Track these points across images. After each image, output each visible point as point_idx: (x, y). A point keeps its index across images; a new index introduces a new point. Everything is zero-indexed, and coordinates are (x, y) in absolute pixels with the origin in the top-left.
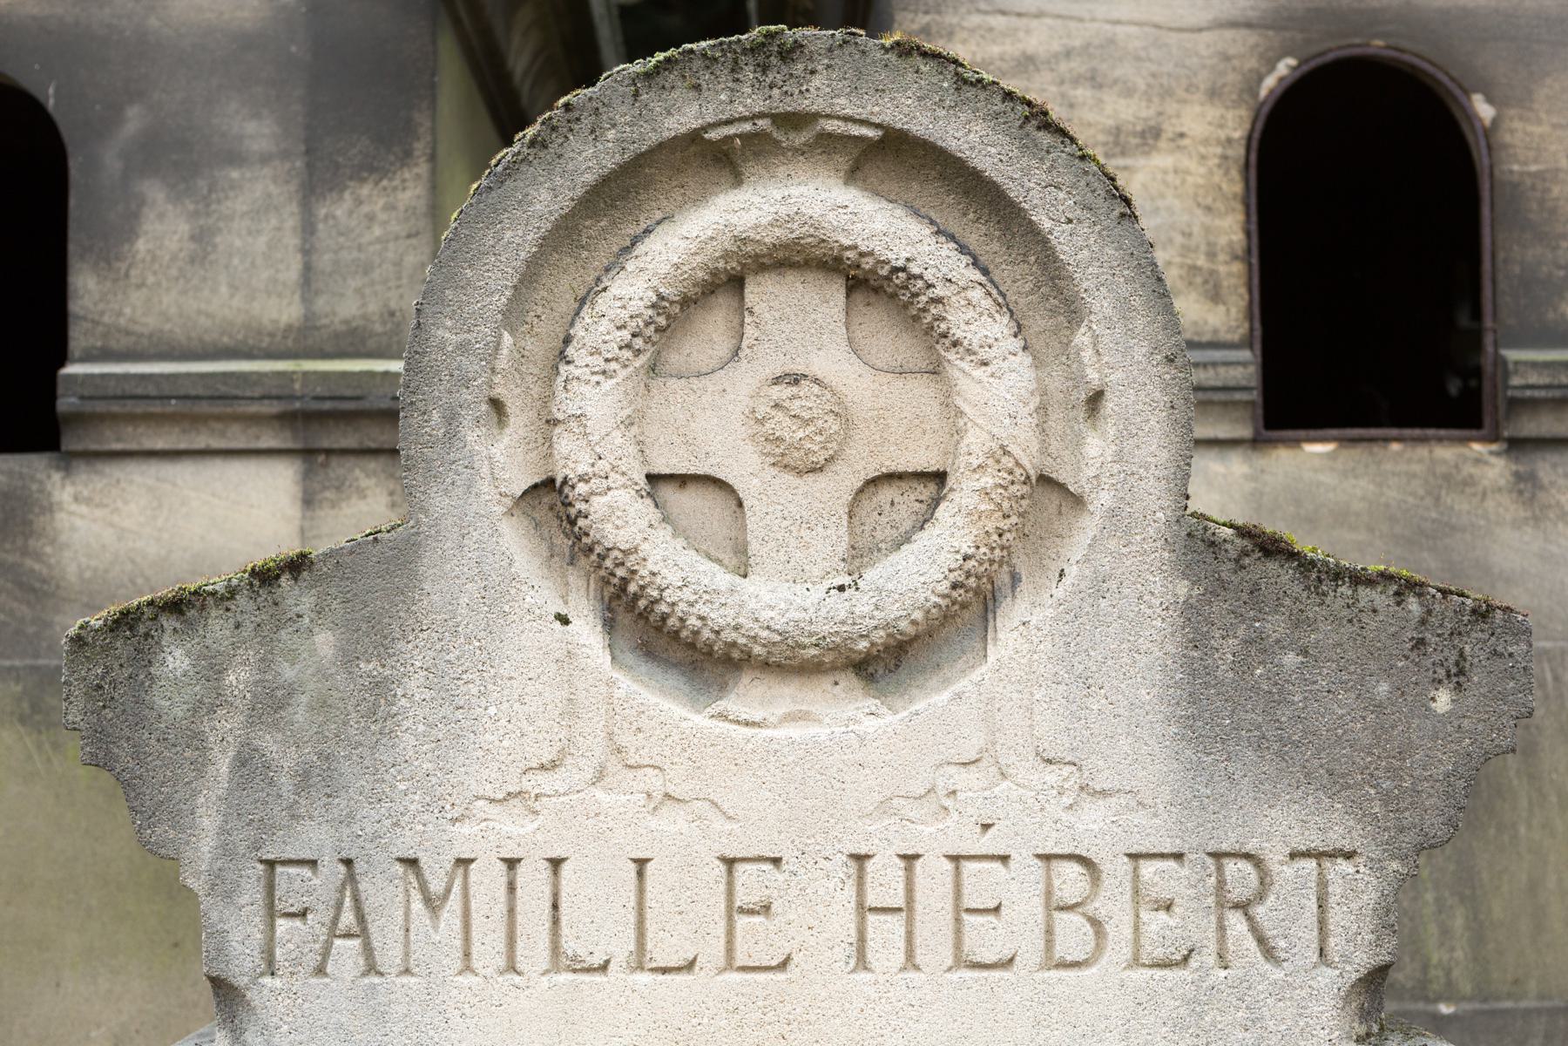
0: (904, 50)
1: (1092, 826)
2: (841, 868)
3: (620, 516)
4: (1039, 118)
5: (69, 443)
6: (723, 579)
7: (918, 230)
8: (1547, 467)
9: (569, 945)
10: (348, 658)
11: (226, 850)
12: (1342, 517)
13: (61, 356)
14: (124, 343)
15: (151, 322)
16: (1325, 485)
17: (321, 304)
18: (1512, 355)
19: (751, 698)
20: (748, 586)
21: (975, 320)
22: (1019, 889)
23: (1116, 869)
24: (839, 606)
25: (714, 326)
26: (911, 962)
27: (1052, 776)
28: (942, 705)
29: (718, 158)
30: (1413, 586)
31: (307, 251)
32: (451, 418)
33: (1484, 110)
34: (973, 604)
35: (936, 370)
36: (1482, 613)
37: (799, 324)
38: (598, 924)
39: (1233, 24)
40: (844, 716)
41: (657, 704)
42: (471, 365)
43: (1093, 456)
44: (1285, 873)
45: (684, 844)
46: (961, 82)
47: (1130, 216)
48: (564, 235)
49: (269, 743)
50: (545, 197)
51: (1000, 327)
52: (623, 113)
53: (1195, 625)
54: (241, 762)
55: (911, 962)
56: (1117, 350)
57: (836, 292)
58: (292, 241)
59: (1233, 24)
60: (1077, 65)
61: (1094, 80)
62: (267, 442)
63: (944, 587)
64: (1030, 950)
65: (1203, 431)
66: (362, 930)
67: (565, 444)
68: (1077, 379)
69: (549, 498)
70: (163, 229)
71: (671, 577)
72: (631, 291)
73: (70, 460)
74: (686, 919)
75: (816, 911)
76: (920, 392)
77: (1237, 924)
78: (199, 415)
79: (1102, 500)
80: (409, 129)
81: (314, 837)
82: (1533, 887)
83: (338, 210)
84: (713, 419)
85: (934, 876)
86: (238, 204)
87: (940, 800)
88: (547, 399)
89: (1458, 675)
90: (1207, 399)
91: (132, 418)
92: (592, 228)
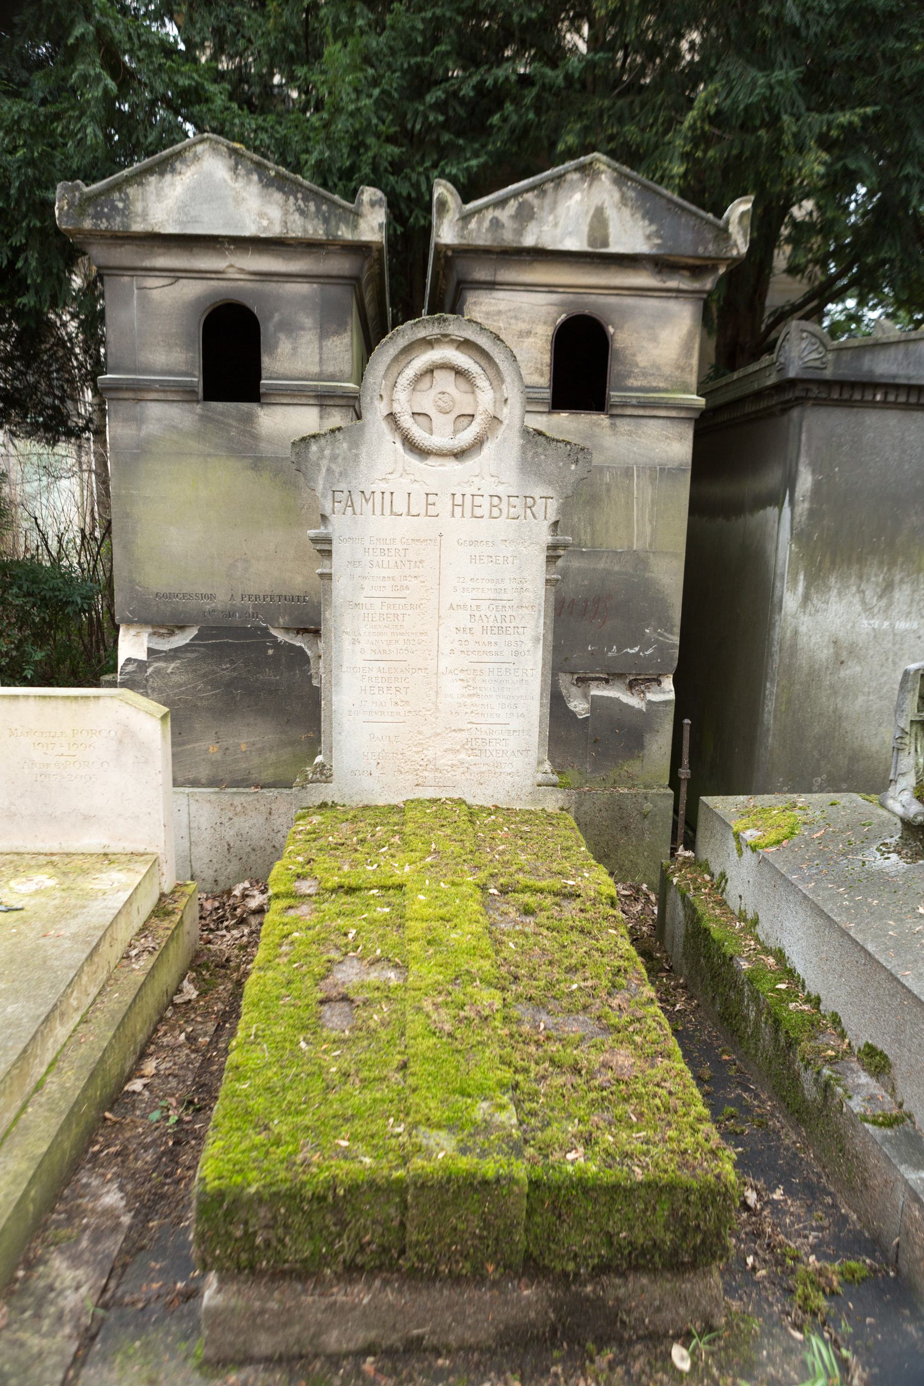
0: (470, 321)
1: (501, 490)
2: (449, 496)
3: (406, 421)
4: (498, 338)
5: (263, 400)
6: (427, 435)
7: (471, 361)
8: (618, 421)
9: (394, 510)
10: (350, 449)
11: (324, 488)
12: (568, 432)
13: (260, 379)
14: (274, 375)
15: (282, 371)
16: (565, 424)
17: (324, 367)
18: (612, 393)
19: (432, 461)
20: (433, 437)
21: (482, 382)
22: (485, 502)
23: (505, 499)
24: (451, 442)
26: (463, 516)
27: (493, 479)
28: (471, 464)
29: (428, 343)
30: (569, 443)
31: (320, 354)
32: (372, 398)
33: (611, 330)
34: (478, 443)
35: (473, 392)
36: (582, 449)
37: (444, 379)
38: (400, 505)
39: (551, 304)
40: (452, 465)
41: (413, 461)
42: (376, 387)
43: (505, 413)
44: (539, 501)
45: (419, 491)
46: (481, 329)
47: (515, 360)
48: (396, 359)
49: (333, 466)
51: (487, 383)
52: (409, 332)
54: (328, 470)
55: (463, 516)
56: (512, 390)
57: (453, 374)
58: (317, 351)
59: (551, 304)
60: (512, 314)
61: (516, 318)
62: (312, 402)
64: (487, 515)
65: (528, 409)
66: (352, 506)
67: (395, 405)
68: (502, 396)
69: (392, 417)
70: (284, 346)
71: (417, 434)
72: (410, 372)
73: (262, 405)
74: (418, 506)
75: (444, 505)
76: (469, 397)
77: (528, 511)
78: (295, 394)
79: (506, 422)
80: (346, 323)
81: (343, 486)
82: (607, 523)
83: (328, 343)
84: (426, 402)
85: (468, 498)
86: (303, 340)
87: (470, 483)
88: (391, 395)
89: (577, 462)
90: (530, 400)
91: (279, 395)
92: (402, 357)
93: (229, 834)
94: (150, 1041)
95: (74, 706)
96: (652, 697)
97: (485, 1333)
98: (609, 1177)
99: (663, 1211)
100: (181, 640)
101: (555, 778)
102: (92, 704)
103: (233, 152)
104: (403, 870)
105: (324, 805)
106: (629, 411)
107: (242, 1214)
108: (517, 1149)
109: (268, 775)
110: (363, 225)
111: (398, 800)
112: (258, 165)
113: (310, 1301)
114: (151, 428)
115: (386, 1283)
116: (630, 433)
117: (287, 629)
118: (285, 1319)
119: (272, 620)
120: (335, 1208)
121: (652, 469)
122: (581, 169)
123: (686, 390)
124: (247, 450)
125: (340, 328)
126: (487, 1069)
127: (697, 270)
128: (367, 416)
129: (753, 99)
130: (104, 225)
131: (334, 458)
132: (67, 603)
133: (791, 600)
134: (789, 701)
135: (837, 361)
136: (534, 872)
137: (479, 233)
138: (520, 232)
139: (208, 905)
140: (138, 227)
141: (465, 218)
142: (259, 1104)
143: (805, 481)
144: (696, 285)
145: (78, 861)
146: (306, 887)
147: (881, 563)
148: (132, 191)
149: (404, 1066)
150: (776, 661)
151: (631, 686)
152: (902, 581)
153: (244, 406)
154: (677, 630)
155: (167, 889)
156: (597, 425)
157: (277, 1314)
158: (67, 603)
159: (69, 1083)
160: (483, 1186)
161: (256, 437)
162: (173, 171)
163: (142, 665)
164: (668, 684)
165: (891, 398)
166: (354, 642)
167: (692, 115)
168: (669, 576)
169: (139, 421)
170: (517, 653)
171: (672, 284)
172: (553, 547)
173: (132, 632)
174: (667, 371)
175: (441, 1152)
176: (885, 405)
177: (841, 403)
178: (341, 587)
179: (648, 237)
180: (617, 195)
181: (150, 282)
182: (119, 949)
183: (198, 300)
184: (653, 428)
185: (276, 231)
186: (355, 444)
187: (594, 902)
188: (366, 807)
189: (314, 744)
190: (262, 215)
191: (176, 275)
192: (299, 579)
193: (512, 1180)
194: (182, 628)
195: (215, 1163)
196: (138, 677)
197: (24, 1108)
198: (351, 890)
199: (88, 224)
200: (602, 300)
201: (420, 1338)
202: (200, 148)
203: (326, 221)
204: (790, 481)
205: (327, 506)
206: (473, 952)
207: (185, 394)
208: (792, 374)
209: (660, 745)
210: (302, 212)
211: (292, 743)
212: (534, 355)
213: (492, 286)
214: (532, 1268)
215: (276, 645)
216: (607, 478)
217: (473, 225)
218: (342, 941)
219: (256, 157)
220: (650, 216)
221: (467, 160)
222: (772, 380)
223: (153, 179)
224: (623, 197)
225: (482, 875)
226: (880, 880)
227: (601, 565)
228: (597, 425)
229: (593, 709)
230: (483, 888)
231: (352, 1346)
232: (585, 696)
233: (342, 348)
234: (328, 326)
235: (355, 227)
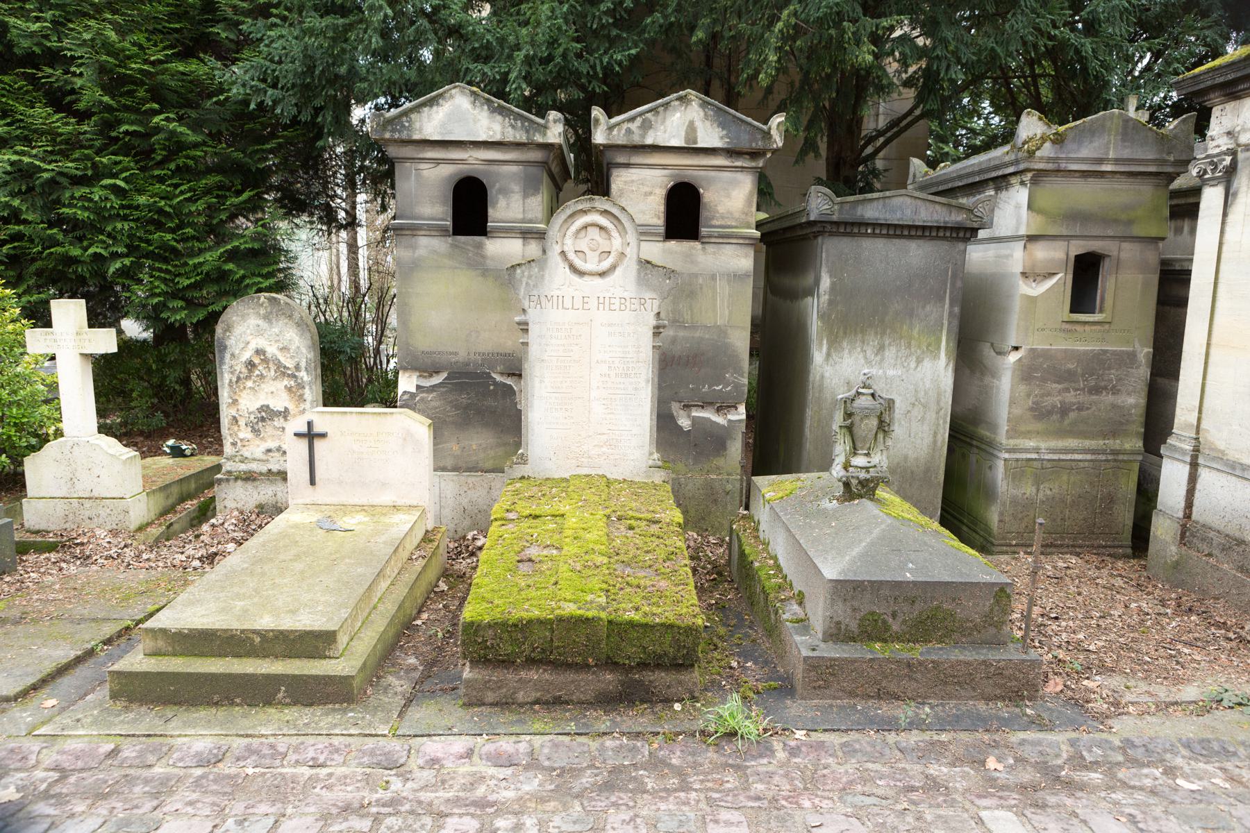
1: (626, 295)
3: (571, 256)
8: (707, 246)
19: (586, 278)
21: (615, 233)
22: (617, 302)
25: (583, 232)
29: (584, 212)
34: (613, 268)
37: (594, 233)
38: (568, 304)
40: (598, 281)
43: (628, 251)
48: (566, 220)
50: (563, 216)
53: (639, 272)
63: (533, 315)
70: (502, 203)
72: (574, 228)
74: (578, 304)
75: (593, 303)
78: (507, 232)
81: (535, 292)
83: (528, 201)
84: (583, 245)
85: (607, 300)
87: (608, 291)
93: (465, 502)
94: (423, 606)
95: (378, 418)
96: (731, 417)
97: (589, 696)
98: (644, 621)
99: (669, 638)
100: (437, 380)
101: (660, 463)
102: (389, 417)
103: (473, 93)
104: (564, 508)
105: (523, 478)
106: (713, 240)
107: (481, 633)
108: (604, 609)
109: (489, 465)
110: (549, 133)
111: (566, 475)
112: (488, 100)
113: (510, 676)
114: (421, 252)
115: (545, 670)
116: (714, 253)
117: (502, 374)
118: (500, 685)
119: (493, 368)
120: (522, 630)
121: (729, 275)
122: (680, 99)
123: (749, 227)
124: (480, 265)
125: (536, 191)
126: (595, 583)
127: (754, 154)
128: (549, 253)
129: (820, 14)
130: (397, 136)
131: (530, 277)
132: (340, 352)
133: (818, 356)
134: (819, 421)
135: (840, 210)
136: (638, 510)
137: (619, 137)
138: (643, 136)
139: (452, 545)
140: (416, 137)
141: (611, 128)
142: (488, 596)
143: (826, 282)
144: (753, 164)
145: (379, 510)
146: (511, 516)
147: (876, 333)
148: (413, 116)
149: (556, 583)
150: (811, 396)
151: (718, 410)
152: (890, 345)
153: (477, 238)
154: (746, 375)
155: (430, 528)
156: (693, 248)
157: (496, 683)
158: (340, 352)
159: (389, 608)
160: (587, 621)
161: (483, 257)
162: (438, 104)
163: (413, 395)
164: (742, 409)
165: (877, 231)
166: (541, 382)
167: (780, 25)
168: (741, 341)
169: (414, 247)
170: (636, 389)
171: (738, 164)
172: (657, 327)
173: (407, 375)
174: (737, 215)
175: (570, 609)
176: (874, 235)
177: (845, 234)
178: (534, 350)
179: (722, 138)
180: (702, 114)
181: (422, 166)
182: (406, 555)
183: (451, 176)
184: (728, 251)
185: (498, 138)
186: (542, 269)
187: (668, 524)
188: (547, 479)
189: (518, 445)
190: (489, 129)
191: (437, 162)
192: (510, 343)
193: (600, 619)
194: (437, 372)
195: (468, 614)
196: (410, 403)
197: (370, 614)
198: (536, 517)
199: (387, 135)
200: (696, 173)
201: (560, 697)
202: (453, 91)
203: (527, 132)
204: (817, 282)
205: (526, 304)
206: (596, 542)
207: (442, 232)
208: (812, 218)
209: (736, 450)
210: (513, 127)
211: (505, 445)
212: (652, 209)
213: (627, 166)
214: (610, 664)
215: (495, 383)
216: (700, 281)
217: (615, 132)
218: (529, 538)
219: (487, 95)
220: (722, 125)
221: (630, 49)
222: (804, 220)
223: (426, 109)
224: (706, 114)
225: (608, 511)
226: (824, 513)
227: (698, 334)
228: (693, 248)
229: (693, 425)
230: (608, 517)
231: (529, 700)
232: (689, 416)
233: (537, 204)
234: (530, 188)
235: (545, 135)
